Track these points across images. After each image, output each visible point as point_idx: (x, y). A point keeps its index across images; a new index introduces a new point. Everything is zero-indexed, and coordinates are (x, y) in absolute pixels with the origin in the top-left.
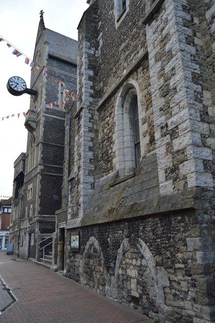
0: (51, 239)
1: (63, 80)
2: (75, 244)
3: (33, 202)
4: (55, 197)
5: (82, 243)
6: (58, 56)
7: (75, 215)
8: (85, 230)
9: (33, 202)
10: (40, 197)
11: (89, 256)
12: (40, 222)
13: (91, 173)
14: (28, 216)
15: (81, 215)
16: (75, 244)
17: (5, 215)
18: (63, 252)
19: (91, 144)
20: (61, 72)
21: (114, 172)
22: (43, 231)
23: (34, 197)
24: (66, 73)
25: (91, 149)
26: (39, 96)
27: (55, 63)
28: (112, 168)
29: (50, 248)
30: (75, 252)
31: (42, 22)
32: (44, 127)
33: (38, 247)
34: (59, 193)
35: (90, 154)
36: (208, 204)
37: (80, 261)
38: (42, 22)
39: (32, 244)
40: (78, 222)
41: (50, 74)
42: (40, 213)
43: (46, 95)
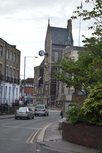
0: (54, 102)
1: (57, 51)
2: (59, 103)
3: (48, 91)
4: (54, 90)
5: (60, 103)
6: (55, 44)
7: (59, 99)
8: (60, 101)
9: (48, 91)
10: (50, 90)
11: (60, 105)
12: (51, 98)
13: (61, 93)
14: (46, 94)
15: (60, 99)
16: (59, 103)
17: (26, 88)
18: (57, 104)
19: (62, 88)
20: (56, 49)
21: (64, 94)
22: (52, 100)
23: (48, 89)
24: (57, 49)
25: (62, 89)
26: (49, 55)
27: (54, 46)
28: (64, 93)
29: (54, 104)
30: (59, 104)
31: (49, 24)
32: (51, 69)
33: (51, 104)
34: (55, 89)
35: (61, 90)
36: (98, 62)
37: (59, 105)
38: (49, 24)
39: (49, 103)
40: (59, 100)
42: (50, 95)
43: (51, 58)
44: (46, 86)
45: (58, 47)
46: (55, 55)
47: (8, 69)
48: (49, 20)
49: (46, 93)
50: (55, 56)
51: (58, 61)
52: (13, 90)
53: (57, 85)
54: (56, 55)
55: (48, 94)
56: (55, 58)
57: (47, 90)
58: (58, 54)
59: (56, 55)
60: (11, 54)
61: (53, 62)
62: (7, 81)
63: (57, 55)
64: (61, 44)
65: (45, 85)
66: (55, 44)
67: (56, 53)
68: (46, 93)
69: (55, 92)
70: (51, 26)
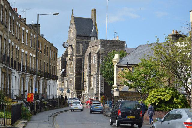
1: (81, 43)
2: (86, 97)
4: (80, 83)
5: (88, 97)
6: (80, 35)
16: (86, 97)
20: (80, 40)
27: (79, 38)
30: (86, 98)
32: (76, 61)
34: (81, 82)
41: (78, 42)
42: (75, 88)
44: (71, 79)
45: (83, 38)
46: (80, 47)
47: (13, 49)
48: (73, 10)
49: (71, 86)
50: (79, 47)
51: (83, 53)
52: (54, 86)
53: (82, 78)
54: (81, 47)
55: (73, 87)
56: (80, 50)
57: (71, 83)
58: (83, 46)
59: (81, 47)
60: (23, 34)
61: (77, 54)
62: (51, 79)
63: (82, 47)
64: (86, 35)
65: (70, 78)
66: (90, 79)
67: (81, 44)
68: (71, 86)
69: (80, 85)
70: (75, 16)
